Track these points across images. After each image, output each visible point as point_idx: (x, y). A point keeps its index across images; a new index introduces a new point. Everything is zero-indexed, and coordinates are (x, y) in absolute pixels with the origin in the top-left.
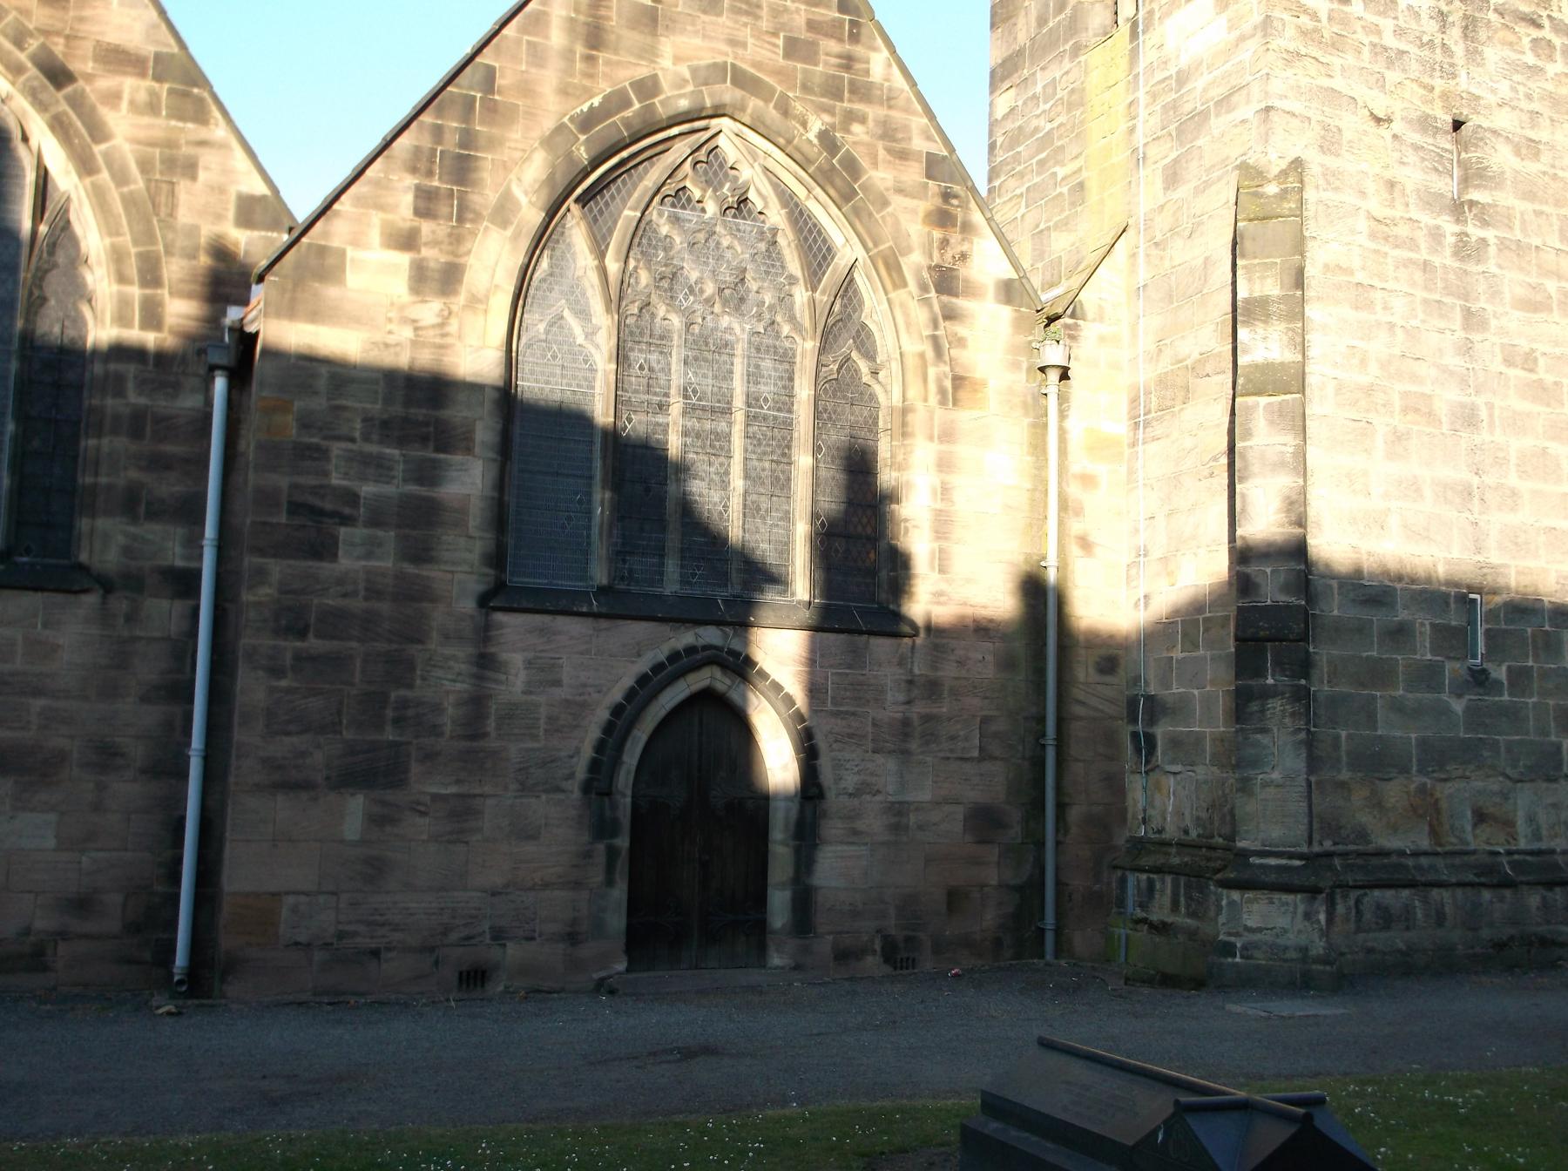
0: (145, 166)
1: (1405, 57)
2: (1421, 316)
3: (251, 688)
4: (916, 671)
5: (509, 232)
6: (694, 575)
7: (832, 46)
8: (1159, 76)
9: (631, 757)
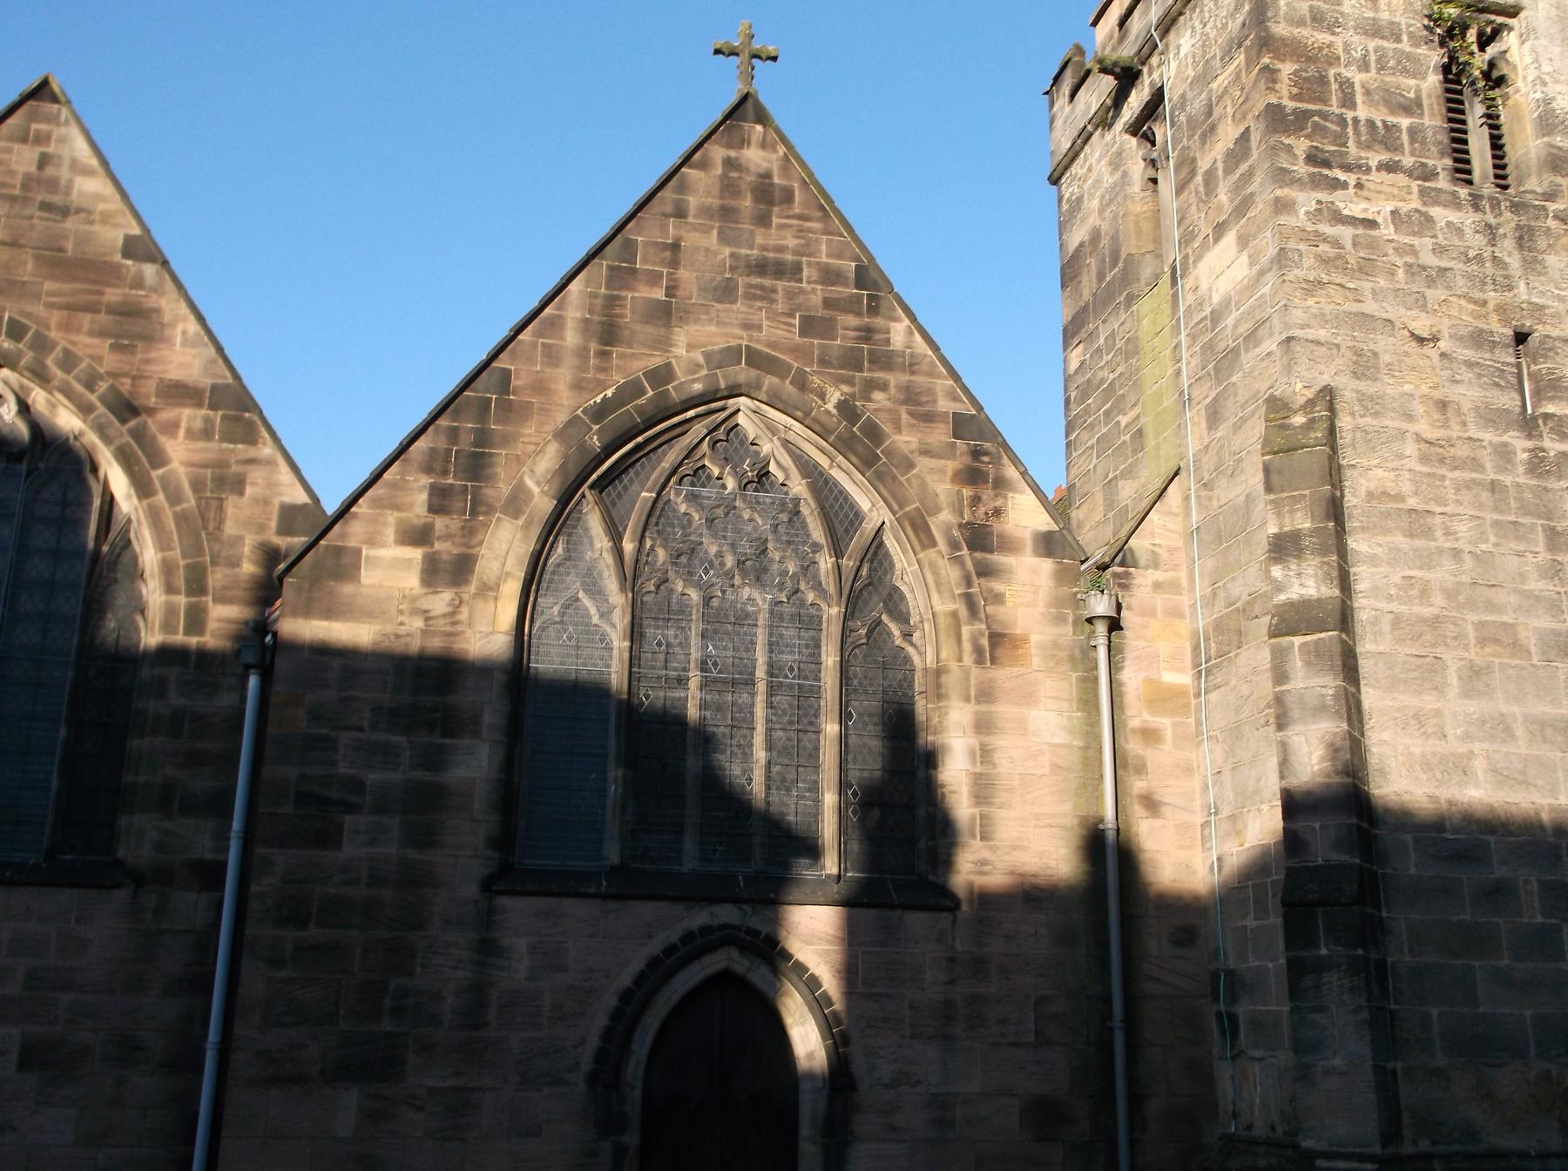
0: (197, 485)
1: (1448, 274)
2: (1493, 539)
3: (255, 982)
4: (959, 948)
5: (520, 522)
6: (715, 851)
7: (852, 320)
8: (1197, 318)
9: (641, 1046)
